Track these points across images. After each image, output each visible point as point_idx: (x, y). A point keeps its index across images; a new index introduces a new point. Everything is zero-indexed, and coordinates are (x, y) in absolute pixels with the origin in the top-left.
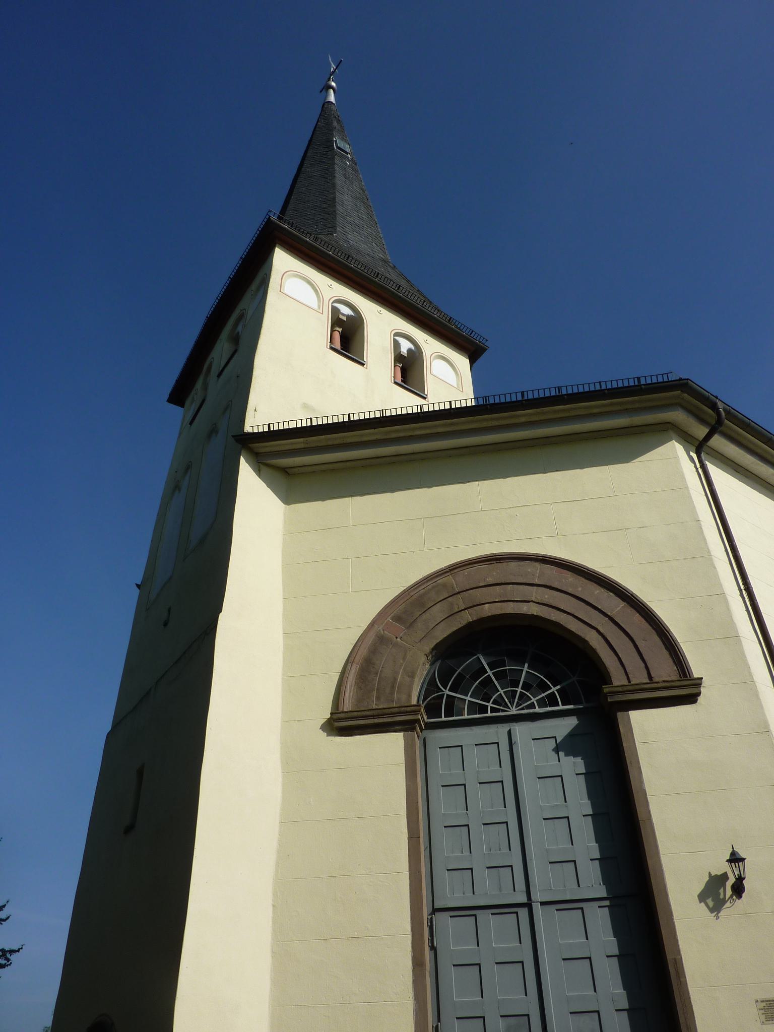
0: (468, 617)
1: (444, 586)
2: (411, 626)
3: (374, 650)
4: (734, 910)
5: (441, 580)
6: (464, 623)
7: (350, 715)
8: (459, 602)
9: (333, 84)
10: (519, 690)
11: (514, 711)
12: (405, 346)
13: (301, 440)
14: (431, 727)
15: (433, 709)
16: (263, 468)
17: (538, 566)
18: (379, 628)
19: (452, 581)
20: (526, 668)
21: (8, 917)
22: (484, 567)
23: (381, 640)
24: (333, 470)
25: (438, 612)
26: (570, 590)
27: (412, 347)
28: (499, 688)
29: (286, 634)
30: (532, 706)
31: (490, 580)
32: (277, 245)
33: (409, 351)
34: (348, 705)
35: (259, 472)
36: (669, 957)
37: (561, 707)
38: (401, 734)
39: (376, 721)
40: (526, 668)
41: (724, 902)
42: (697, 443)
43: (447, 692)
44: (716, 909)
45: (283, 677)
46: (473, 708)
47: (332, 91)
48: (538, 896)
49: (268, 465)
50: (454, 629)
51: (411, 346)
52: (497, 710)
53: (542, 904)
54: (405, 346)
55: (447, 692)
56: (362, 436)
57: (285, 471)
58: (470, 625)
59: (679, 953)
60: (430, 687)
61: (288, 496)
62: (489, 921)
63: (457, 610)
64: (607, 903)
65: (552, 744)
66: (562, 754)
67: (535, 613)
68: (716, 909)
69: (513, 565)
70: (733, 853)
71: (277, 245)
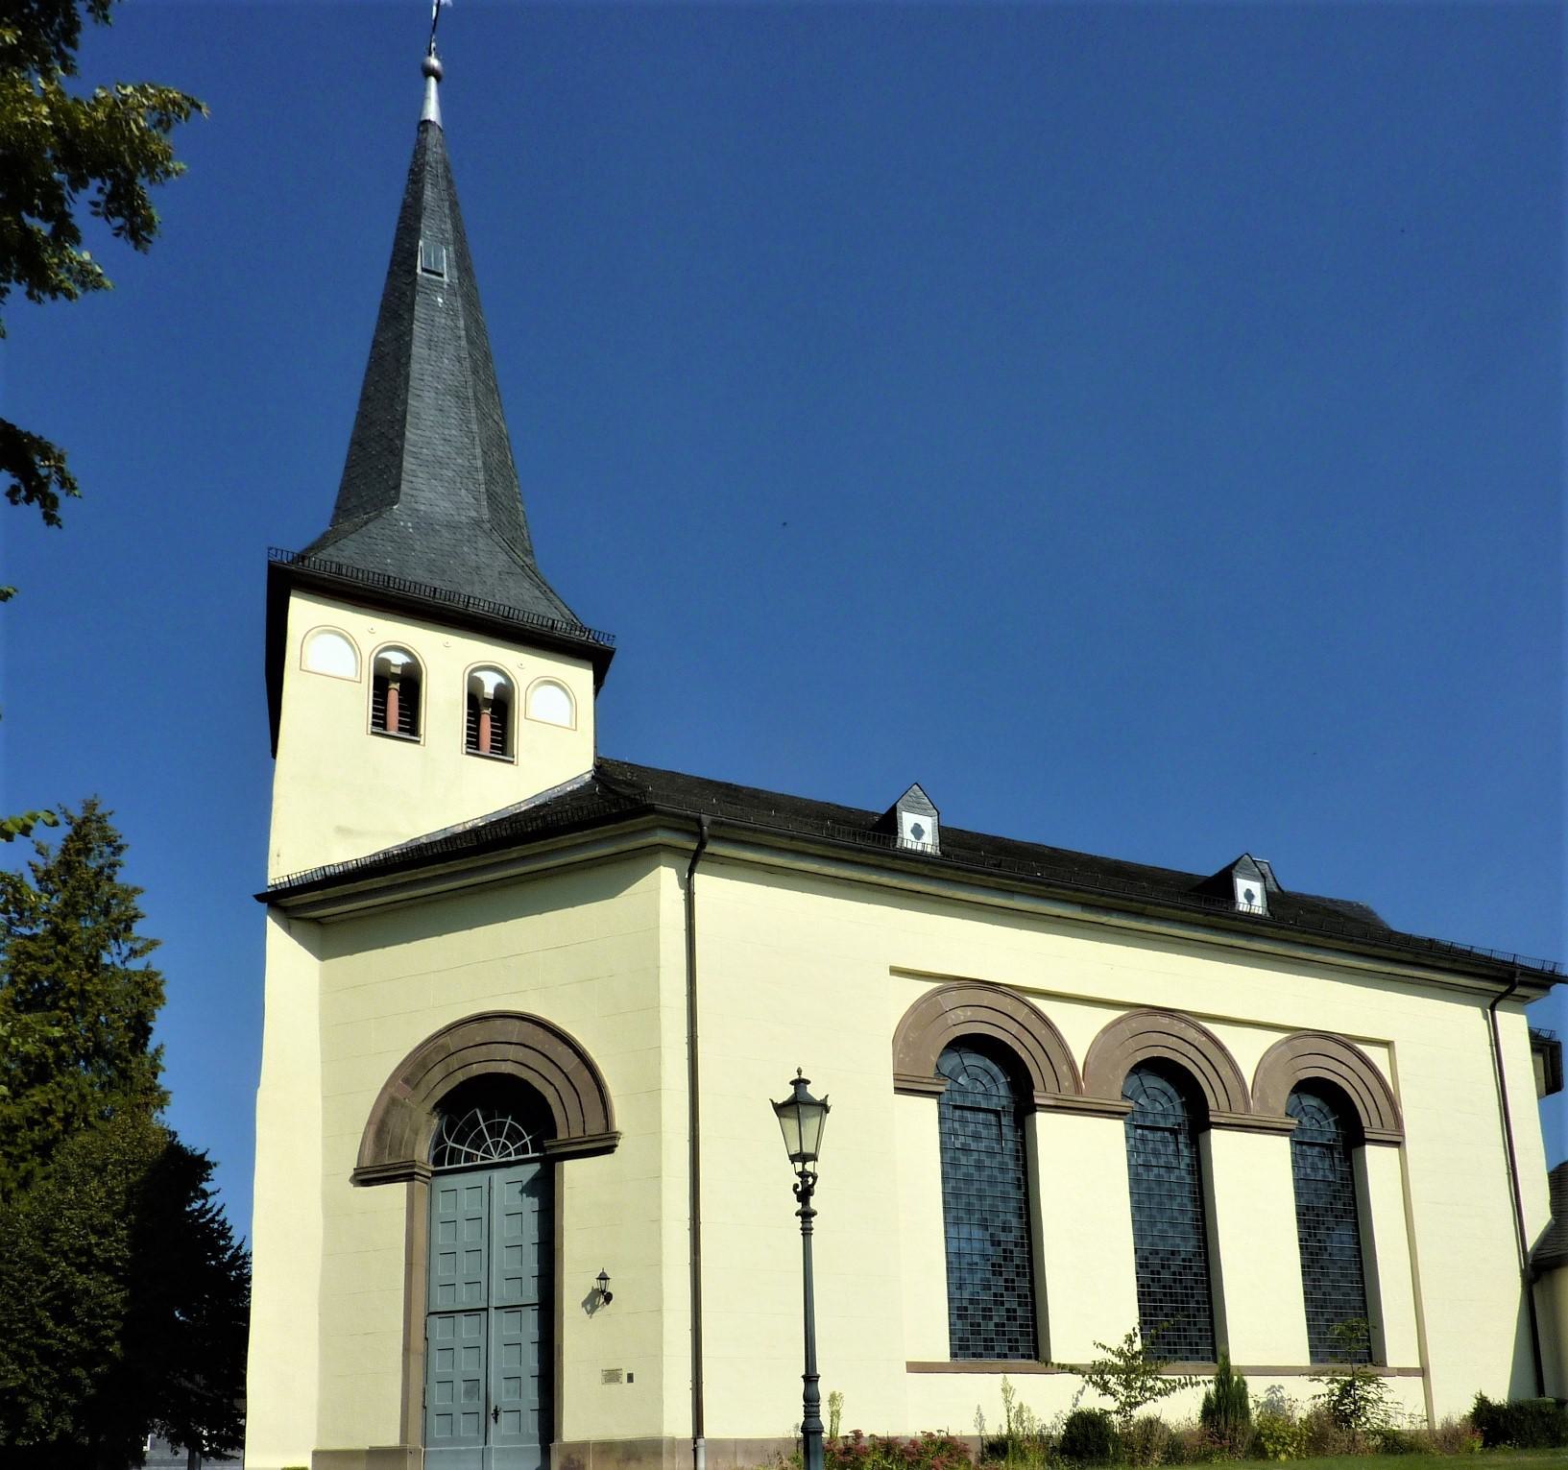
0: (460, 1077)
1: (442, 1046)
2: (416, 1087)
3: (387, 1112)
4: (604, 1311)
5: (441, 1041)
6: (457, 1083)
7: (366, 1170)
8: (454, 1062)
9: (434, 62)
10: (489, 1141)
11: (496, 1159)
12: (490, 684)
13: (318, 892)
14: (436, 1174)
15: (438, 1160)
17: (518, 1023)
18: (391, 1090)
19: (452, 1042)
20: (509, 1121)
22: (475, 1025)
23: (393, 1101)
24: (352, 919)
25: (437, 1073)
26: (539, 1048)
28: (461, 1147)
29: (324, 1098)
30: (510, 1154)
31: (478, 1040)
32: (293, 592)
33: (499, 688)
34: (366, 1163)
35: (288, 929)
36: (556, 1343)
38: (405, 1183)
39: (375, 1175)
40: (509, 1121)
41: (597, 1307)
42: (692, 855)
44: (591, 1312)
45: (324, 1137)
46: (469, 1157)
47: (432, 80)
48: (494, 1303)
49: (297, 919)
50: (449, 1089)
51: (500, 679)
52: (486, 1159)
53: (496, 1308)
54: (490, 684)
55: (450, 1144)
56: (372, 884)
57: (317, 921)
58: (462, 1084)
59: (562, 1342)
60: (439, 1141)
61: (323, 952)
62: (462, 1319)
63: (451, 1070)
64: (537, 1307)
65: (519, 1187)
66: (524, 1195)
67: (510, 1071)
68: (591, 1312)
69: (499, 1022)
70: (603, 1273)
71: (293, 592)
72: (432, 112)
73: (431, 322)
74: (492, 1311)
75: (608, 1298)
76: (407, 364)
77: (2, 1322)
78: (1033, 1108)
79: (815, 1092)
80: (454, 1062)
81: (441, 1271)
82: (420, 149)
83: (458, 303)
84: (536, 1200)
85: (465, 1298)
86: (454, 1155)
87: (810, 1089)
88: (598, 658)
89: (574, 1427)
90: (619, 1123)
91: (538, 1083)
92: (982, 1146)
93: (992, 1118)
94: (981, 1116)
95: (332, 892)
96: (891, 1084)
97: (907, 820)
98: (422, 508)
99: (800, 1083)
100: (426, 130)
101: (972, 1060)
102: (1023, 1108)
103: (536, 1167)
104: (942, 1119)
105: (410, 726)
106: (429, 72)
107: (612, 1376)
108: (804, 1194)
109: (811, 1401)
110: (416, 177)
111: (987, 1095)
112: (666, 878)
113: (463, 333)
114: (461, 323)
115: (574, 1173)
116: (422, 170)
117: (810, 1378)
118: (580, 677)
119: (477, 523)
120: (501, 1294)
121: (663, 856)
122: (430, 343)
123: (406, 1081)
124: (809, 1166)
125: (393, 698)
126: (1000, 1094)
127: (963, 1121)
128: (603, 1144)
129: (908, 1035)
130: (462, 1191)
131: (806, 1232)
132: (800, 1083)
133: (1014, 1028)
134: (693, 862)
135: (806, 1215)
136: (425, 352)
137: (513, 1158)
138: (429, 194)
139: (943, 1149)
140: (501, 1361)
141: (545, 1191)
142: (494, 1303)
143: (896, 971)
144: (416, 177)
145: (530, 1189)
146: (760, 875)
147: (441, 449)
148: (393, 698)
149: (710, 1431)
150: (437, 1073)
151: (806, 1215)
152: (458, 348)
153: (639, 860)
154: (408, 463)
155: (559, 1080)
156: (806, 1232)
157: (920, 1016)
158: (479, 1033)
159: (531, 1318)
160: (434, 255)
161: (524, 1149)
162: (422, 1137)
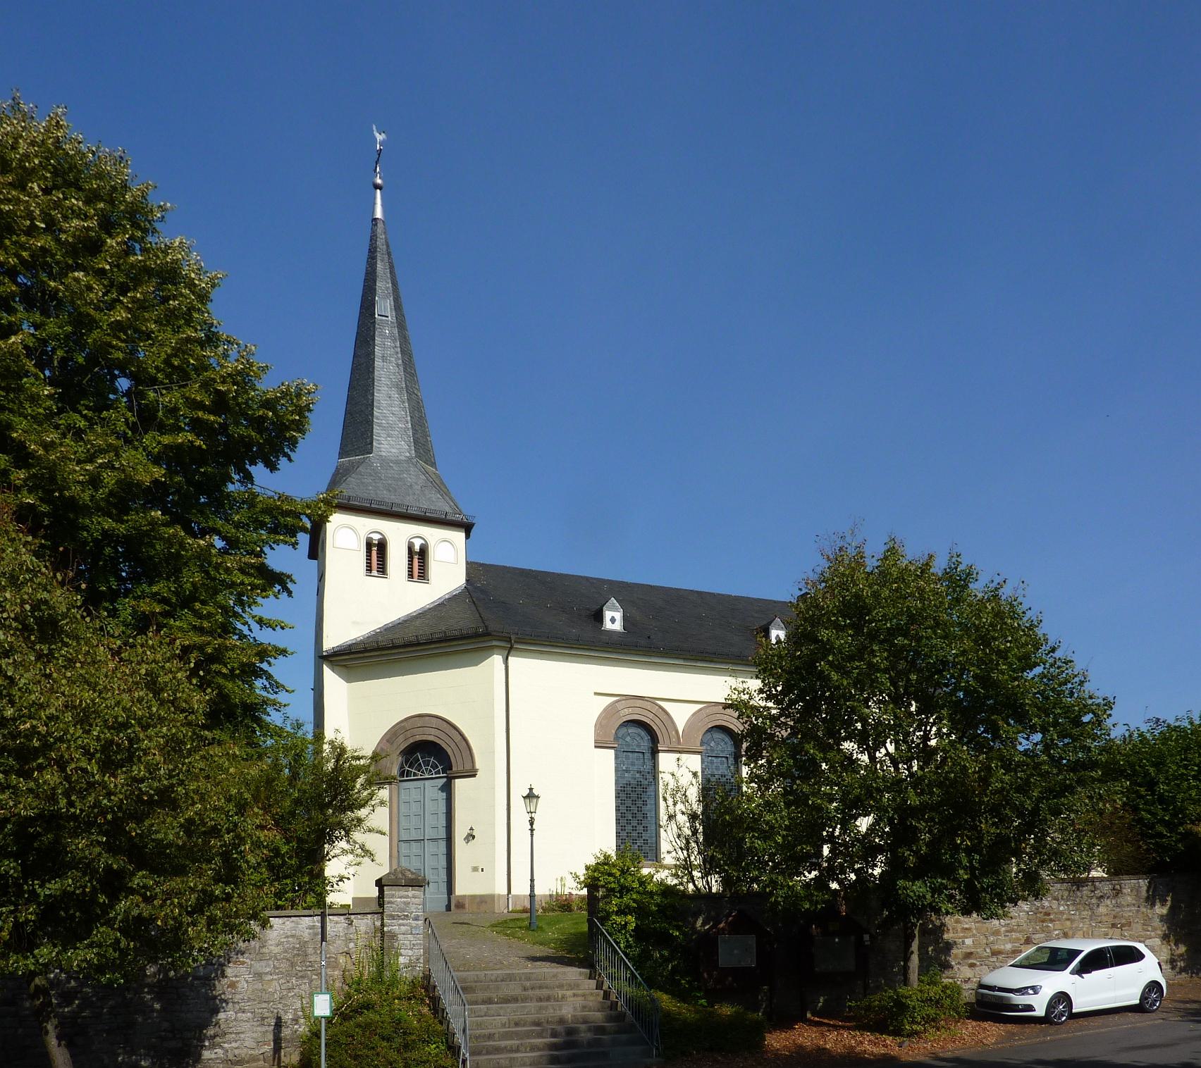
0: (411, 741)
4: (472, 842)
8: (408, 734)
9: (379, 181)
12: (417, 545)
14: (400, 781)
15: (402, 774)
16: (335, 667)
18: (381, 745)
19: (407, 725)
21: (293, 691)
25: (401, 738)
27: (423, 542)
37: (441, 775)
43: (407, 768)
46: (415, 775)
48: (426, 837)
55: (407, 768)
60: (402, 767)
61: (349, 680)
68: (467, 843)
69: (427, 718)
72: (379, 214)
73: (384, 347)
74: (426, 841)
75: (474, 837)
76: (373, 372)
77: (1, 800)
78: (658, 751)
79: (535, 792)
80: (408, 734)
81: (404, 824)
82: (373, 238)
83: (396, 331)
84: (445, 794)
85: (414, 836)
86: (408, 774)
87: (534, 791)
88: (467, 528)
89: (461, 889)
90: (478, 766)
91: (444, 746)
92: (635, 768)
93: (641, 755)
94: (636, 754)
95: (352, 656)
96: (593, 744)
97: (608, 615)
98: (384, 454)
99: (531, 789)
100: (376, 225)
101: (632, 730)
102: (654, 752)
103: (445, 780)
104: (616, 758)
105: (382, 569)
106: (377, 187)
107: (475, 869)
108: (532, 823)
109: (532, 887)
110: (372, 252)
111: (639, 746)
112: (497, 660)
113: (399, 349)
114: (398, 344)
115: (459, 784)
116: (376, 251)
117: (532, 880)
118: (459, 536)
119: (410, 459)
120: (430, 833)
121: (496, 650)
122: (384, 358)
123: (388, 741)
124: (533, 815)
125: (374, 554)
126: (645, 744)
127: (627, 758)
128: (472, 773)
129: (601, 725)
130: (411, 790)
131: (532, 835)
132: (531, 789)
133: (651, 716)
134: (509, 651)
135: (532, 830)
136: (381, 364)
137: (434, 776)
138: (380, 266)
139: (617, 770)
140: (430, 863)
141: (448, 789)
142: (426, 837)
143: (596, 694)
144: (372, 252)
145: (443, 789)
146: (537, 655)
147: (392, 419)
148: (374, 554)
149: (513, 892)
150: (401, 738)
151: (532, 830)
152: (397, 359)
153: (485, 652)
154: (376, 430)
155: (453, 745)
156: (532, 835)
157: (609, 712)
158: (420, 722)
159: (443, 844)
160: (384, 307)
161: (438, 772)
162: (394, 765)
